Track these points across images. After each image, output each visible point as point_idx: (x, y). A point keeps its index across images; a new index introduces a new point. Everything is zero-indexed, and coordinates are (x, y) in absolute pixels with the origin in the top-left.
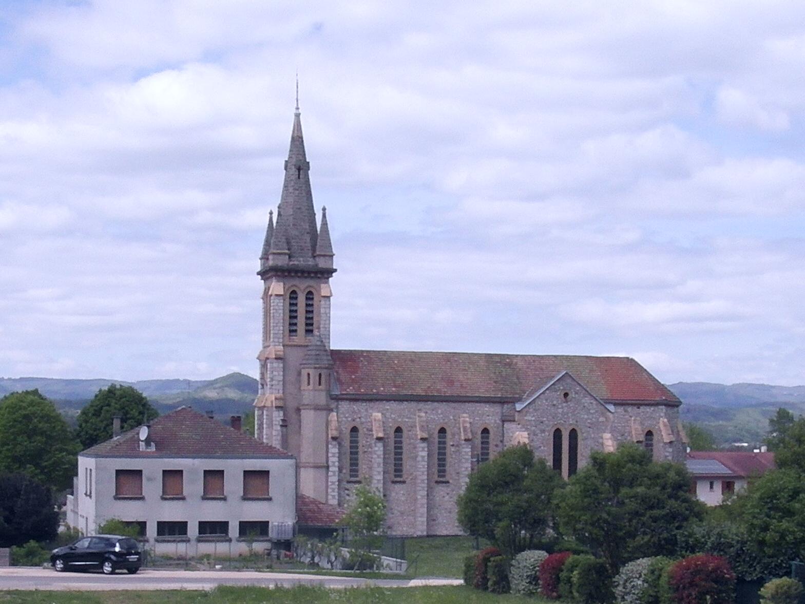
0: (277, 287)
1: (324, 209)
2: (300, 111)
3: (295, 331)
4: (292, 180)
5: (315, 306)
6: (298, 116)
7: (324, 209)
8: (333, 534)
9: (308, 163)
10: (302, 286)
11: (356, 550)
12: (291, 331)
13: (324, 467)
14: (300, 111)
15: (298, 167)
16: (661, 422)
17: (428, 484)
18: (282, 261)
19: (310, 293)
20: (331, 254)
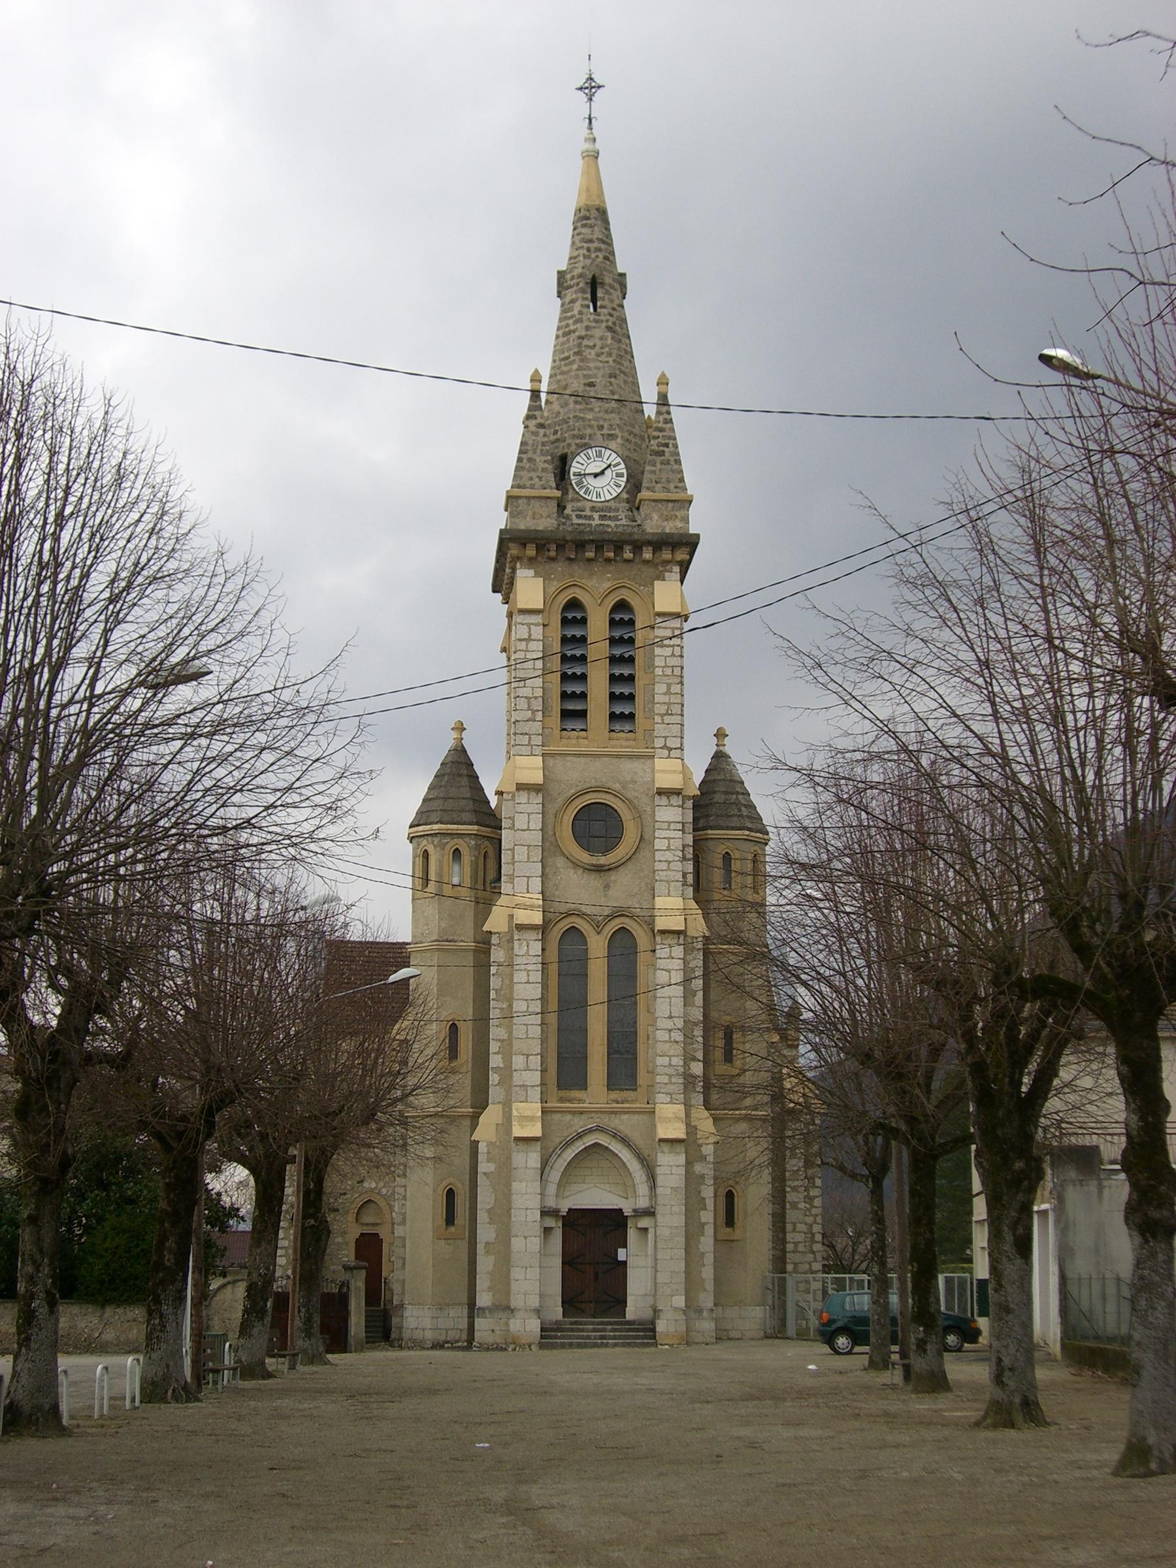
0: (530, 588)
1: (663, 381)
2: (598, 145)
3: (582, 714)
4: (573, 301)
5: (640, 682)
6: (593, 156)
7: (663, 381)
8: (222, 1215)
9: (623, 275)
10: (597, 591)
11: (33, 758)
12: (566, 714)
13: (530, 635)
14: (598, 145)
15: (594, 285)
16: (934, 1102)
17: (785, 1171)
18: (543, 521)
19: (622, 606)
20: (680, 496)
